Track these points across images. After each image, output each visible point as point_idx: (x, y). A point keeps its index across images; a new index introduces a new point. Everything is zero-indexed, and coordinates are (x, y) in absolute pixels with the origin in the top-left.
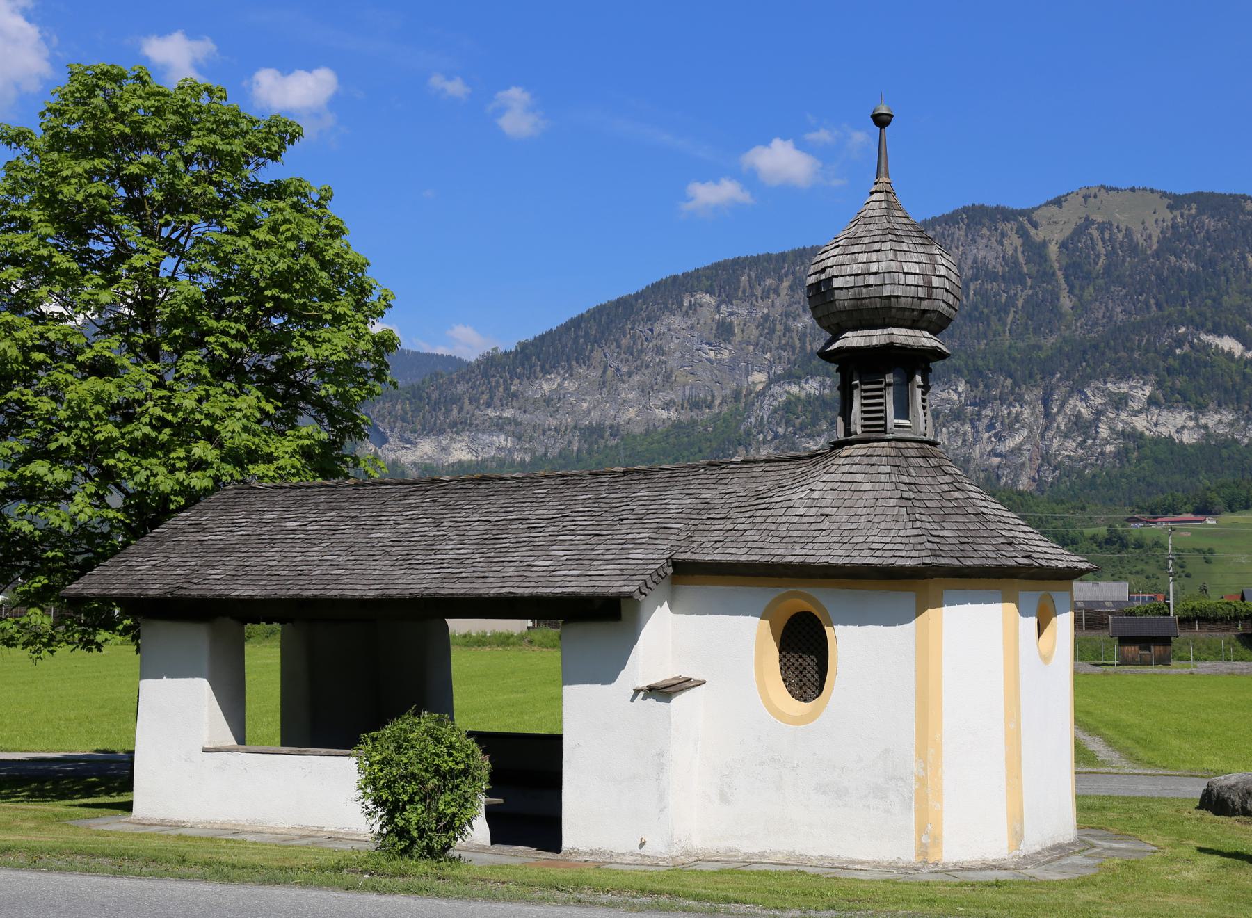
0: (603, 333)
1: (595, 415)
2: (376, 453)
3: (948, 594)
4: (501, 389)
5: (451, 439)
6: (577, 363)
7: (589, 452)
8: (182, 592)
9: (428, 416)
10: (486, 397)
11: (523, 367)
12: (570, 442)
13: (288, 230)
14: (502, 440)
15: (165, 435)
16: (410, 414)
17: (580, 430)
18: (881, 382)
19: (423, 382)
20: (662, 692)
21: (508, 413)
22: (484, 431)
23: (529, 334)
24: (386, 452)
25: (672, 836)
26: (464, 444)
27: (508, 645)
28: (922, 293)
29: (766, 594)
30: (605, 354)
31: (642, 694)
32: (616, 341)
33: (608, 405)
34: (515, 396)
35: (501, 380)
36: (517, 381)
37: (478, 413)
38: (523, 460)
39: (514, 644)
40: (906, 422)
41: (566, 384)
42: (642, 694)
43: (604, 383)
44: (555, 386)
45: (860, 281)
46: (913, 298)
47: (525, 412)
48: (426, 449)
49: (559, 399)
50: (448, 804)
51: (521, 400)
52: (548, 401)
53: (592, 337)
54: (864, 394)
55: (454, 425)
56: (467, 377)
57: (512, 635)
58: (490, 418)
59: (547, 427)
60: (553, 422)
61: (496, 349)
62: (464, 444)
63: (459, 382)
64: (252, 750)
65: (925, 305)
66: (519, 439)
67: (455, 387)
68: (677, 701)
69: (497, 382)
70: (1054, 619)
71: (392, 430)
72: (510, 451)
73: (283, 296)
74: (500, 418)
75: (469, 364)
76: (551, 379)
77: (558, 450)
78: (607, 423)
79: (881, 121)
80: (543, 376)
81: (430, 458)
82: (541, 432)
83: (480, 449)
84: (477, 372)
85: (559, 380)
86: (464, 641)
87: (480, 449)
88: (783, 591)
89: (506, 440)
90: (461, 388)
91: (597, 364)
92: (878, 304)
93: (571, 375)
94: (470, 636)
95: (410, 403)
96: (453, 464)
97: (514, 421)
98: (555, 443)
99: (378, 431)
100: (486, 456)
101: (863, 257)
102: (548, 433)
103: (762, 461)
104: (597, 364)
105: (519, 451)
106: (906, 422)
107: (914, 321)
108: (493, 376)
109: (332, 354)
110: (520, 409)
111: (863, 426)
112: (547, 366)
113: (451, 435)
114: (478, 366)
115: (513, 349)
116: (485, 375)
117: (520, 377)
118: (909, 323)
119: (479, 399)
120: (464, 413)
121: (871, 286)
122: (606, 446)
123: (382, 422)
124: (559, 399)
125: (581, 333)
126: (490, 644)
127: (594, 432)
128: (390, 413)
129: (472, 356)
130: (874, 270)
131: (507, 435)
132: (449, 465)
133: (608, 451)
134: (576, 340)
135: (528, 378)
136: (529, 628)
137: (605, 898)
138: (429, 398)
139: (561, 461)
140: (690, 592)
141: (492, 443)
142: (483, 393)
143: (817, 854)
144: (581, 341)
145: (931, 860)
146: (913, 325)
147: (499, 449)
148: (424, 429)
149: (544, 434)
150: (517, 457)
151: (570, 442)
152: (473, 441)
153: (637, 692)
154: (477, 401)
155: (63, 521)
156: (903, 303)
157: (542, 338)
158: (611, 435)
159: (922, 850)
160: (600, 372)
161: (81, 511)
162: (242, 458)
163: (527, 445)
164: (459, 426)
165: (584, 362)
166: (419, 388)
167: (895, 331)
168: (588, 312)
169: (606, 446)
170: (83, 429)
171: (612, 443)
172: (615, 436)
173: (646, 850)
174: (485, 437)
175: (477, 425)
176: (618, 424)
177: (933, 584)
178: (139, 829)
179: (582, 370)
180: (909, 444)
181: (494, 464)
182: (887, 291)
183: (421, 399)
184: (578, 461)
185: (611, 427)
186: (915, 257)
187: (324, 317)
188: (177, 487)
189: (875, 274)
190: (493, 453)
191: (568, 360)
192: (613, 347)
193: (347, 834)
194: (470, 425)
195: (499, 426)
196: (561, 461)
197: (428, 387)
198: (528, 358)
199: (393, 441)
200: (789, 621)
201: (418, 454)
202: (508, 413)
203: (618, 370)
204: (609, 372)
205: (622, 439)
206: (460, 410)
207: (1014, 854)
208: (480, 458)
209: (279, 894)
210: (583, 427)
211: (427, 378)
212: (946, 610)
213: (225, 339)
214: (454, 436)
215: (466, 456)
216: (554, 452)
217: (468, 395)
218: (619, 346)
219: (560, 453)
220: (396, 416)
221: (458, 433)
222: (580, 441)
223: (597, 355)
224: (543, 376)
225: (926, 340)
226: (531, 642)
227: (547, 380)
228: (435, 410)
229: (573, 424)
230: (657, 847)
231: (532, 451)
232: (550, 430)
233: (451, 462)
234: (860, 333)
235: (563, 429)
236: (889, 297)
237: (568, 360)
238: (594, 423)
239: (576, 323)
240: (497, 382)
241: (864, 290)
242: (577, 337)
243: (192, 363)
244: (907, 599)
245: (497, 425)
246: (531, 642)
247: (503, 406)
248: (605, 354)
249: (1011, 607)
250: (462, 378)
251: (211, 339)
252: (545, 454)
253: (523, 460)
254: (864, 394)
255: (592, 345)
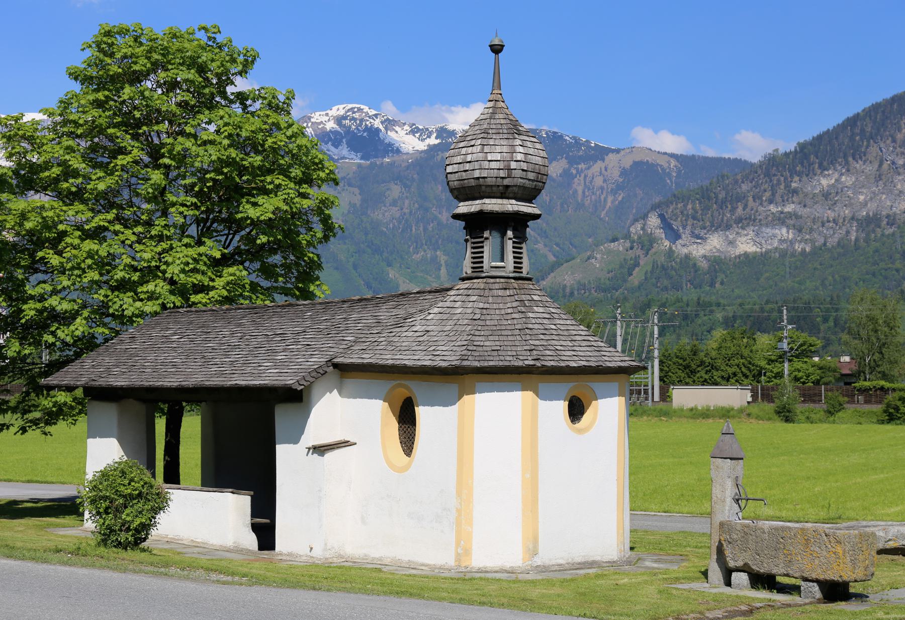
0: (879, 130)
1: (872, 207)
2: (670, 248)
3: (478, 385)
4: (782, 187)
5: (738, 233)
6: (854, 159)
7: (867, 240)
8: (93, 383)
9: (716, 214)
10: (768, 194)
11: (802, 164)
12: (848, 232)
13: (226, 131)
14: (783, 232)
15: (136, 277)
16: (700, 212)
17: (857, 220)
18: (482, 237)
19: (711, 184)
20: (320, 450)
21: (789, 208)
22: (767, 226)
23: (807, 134)
24: (679, 247)
25: (326, 544)
26: (749, 237)
27: (729, 417)
28: (502, 174)
29: (385, 385)
30: (880, 149)
31: (311, 450)
32: (892, 136)
33: (884, 196)
34: (795, 192)
35: (782, 179)
36: (796, 178)
37: (761, 209)
38: (804, 250)
39: (733, 417)
40: (502, 264)
41: (843, 178)
42: (311, 450)
43: (880, 176)
44: (833, 181)
45: (461, 167)
46: (496, 177)
47: (805, 206)
48: (715, 243)
49: (837, 193)
50: (128, 515)
51: (801, 195)
52: (826, 195)
53: (868, 134)
54: (473, 245)
55: (739, 220)
56: (751, 177)
57: (733, 409)
58: (773, 213)
59: (825, 219)
60: (831, 214)
61: (777, 150)
62: (749, 237)
63: (743, 182)
64: (191, 487)
65: (506, 182)
66: (800, 231)
67: (740, 187)
68: (329, 456)
69: (779, 180)
70: (594, 402)
71: (684, 227)
72: (792, 242)
73: (217, 177)
74: (782, 212)
75: (752, 165)
76: (829, 175)
77: (836, 240)
78: (884, 213)
79: (496, 49)
80: (821, 173)
81: (718, 251)
82: (820, 224)
83: (763, 242)
84: (759, 172)
85: (836, 175)
86: (690, 414)
87: (763, 242)
88: (395, 383)
89: (788, 232)
90: (745, 187)
91: (873, 159)
92: (473, 183)
93: (848, 170)
94: (696, 409)
95: (700, 203)
96: (739, 256)
97: (794, 215)
98: (834, 233)
99: (672, 229)
100: (769, 247)
101: (464, 151)
102: (827, 224)
103: (426, 292)
104: (873, 159)
105: (800, 242)
106: (502, 264)
107: (502, 193)
108: (775, 175)
109: (262, 215)
110: (800, 203)
111: (473, 268)
112: (825, 164)
113: (736, 229)
114: (760, 166)
115: (793, 149)
116: (767, 174)
117: (800, 174)
118: (499, 195)
119: (762, 196)
120: (748, 210)
121: (467, 171)
122: (883, 235)
123: (675, 220)
124: (837, 193)
125: (857, 131)
126: (713, 416)
127: (872, 221)
128: (682, 213)
129: (755, 158)
130: (469, 160)
131: (788, 227)
132: (735, 257)
133: (885, 239)
134: (852, 138)
135: (807, 175)
136: (748, 402)
137: (214, 576)
138: (716, 197)
139: (840, 250)
140: (351, 383)
141: (775, 236)
142: (765, 191)
143: (406, 559)
144: (858, 138)
145: (463, 565)
146: (503, 196)
147: (781, 241)
148: (712, 226)
149: (823, 226)
150: (798, 247)
151: (848, 232)
152: (757, 235)
153: (309, 449)
154: (760, 198)
155: (67, 335)
156: (489, 181)
157: (819, 138)
158: (888, 224)
159: (458, 558)
160: (876, 166)
161: (77, 329)
162: (183, 291)
163: (808, 237)
164: (743, 222)
165: (861, 158)
166: (707, 190)
167: (487, 201)
168: (863, 110)
169: (883, 235)
170: (77, 276)
171: (890, 231)
172: (892, 225)
173: (313, 554)
174: (768, 230)
175: (760, 220)
176: (895, 214)
177: (468, 379)
178: (510, 577)
179: (859, 165)
180: (498, 280)
181: (777, 255)
182: (477, 174)
183: (709, 199)
184: (856, 250)
185: (888, 216)
186: (498, 149)
187: (267, 187)
188: (137, 312)
189: (470, 162)
190: (775, 245)
191: (845, 157)
192: (888, 142)
193: (178, 540)
194: (754, 220)
195: (781, 220)
196: (840, 250)
197: (715, 188)
198: (806, 157)
199: (686, 237)
200: (403, 403)
201: (708, 247)
202: (789, 208)
203: (893, 163)
204: (885, 166)
205: (899, 227)
206: (745, 207)
207: (527, 563)
208: (764, 250)
209: (256, 593)
210: (860, 217)
211: (715, 180)
212: (478, 396)
213: (182, 209)
214: (740, 231)
215: (751, 248)
216: (832, 242)
217: (752, 193)
218: (894, 141)
219: (839, 243)
220: (688, 215)
221: (743, 228)
222: (857, 231)
223: (874, 150)
224: (821, 173)
225: (511, 206)
226: (749, 415)
227: (824, 177)
228: (722, 209)
229: (850, 215)
230: (318, 553)
231: (813, 241)
232: (829, 221)
233: (737, 254)
234: (467, 203)
235: (841, 221)
236: (478, 178)
237: (845, 157)
238: (871, 214)
239: (852, 122)
240: (779, 180)
241: (464, 174)
242: (853, 134)
243: (160, 227)
244: (454, 388)
245: (779, 219)
246: (749, 415)
247: (784, 202)
248: (880, 149)
249: (530, 394)
250: (745, 178)
251: (172, 210)
252: (825, 244)
253: (804, 250)
254: (473, 245)
255: (868, 142)
